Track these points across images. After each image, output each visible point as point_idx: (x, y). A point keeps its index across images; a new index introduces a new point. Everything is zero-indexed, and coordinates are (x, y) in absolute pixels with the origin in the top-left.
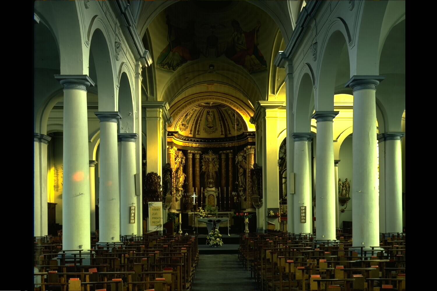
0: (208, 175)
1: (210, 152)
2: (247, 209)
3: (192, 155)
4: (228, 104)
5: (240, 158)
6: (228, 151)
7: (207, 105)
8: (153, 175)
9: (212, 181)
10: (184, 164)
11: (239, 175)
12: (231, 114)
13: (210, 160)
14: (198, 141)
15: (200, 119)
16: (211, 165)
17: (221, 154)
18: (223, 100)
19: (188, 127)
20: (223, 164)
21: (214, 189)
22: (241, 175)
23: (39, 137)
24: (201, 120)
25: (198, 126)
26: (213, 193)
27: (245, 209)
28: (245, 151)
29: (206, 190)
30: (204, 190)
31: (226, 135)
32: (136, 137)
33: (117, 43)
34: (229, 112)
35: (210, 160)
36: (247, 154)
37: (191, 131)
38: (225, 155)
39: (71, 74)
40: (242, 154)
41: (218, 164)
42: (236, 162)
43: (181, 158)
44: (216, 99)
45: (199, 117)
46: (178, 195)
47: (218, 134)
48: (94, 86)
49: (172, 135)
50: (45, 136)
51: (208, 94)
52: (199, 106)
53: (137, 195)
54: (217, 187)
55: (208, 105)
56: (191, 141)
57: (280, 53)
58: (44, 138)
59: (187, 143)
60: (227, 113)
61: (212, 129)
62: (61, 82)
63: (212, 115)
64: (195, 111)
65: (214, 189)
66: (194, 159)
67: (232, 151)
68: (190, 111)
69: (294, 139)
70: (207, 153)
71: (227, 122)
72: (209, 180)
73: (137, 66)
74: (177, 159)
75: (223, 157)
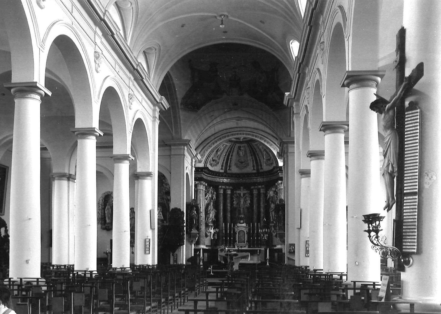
0: (240, 211)
1: (242, 188)
2: (277, 245)
3: (223, 190)
4: (259, 139)
5: (271, 193)
6: (260, 187)
7: (237, 140)
8: (178, 211)
9: (243, 216)
10: (214, 199)
11: (270, 211)
12: (262, 149)
13: (242, 195)
14: (229, 177)
15: (231, 154)
16: (242, 201)
17: (252, 189)
18: (253, 135)
19: (219, 162)
20: (255, 200)
21: (244, 225)
22: (272, 211)
23: (68, 176)
24: (232, 156)
25: (229, 162)
26: (243, 229)
27: (276, 246)
28: (277, 186)
29: (237, 226)
30: (234, 226)
31: (258, 170)
32: (152, 175)
33: (130, 95)
34: (261, 147)
35: (242, 195)
36: (278, 189)
37: (222, 166)
38: (256, 190)
39: (84, 127)
40: (274, 189)
41: (249, 199)
42: (268, 197)
43: (212, 194)
44: (246, 134)
45: (230, 152)
46: (208, 231)
47: (250, 169)
48: (102, 135)
49: (202, 171)
50: (74, 175)
51: (239, 129)
52: (230, 142)
53: (152, 228)
54: (248, 223)
55: (239, 140)
56: (222, 176)
57: (287, 95)
58: (72, 177)
59: (218, 179)
60: (258, 148)
61: (244, 163)
62: (76, 133)
63: (243, 150)
64: (226, 147)
65: (244, 225)
66: (225, 194)
67: (263, 186)
68: (220, 147)
69: (301, 176)
70: (239, 189)
71: (259, 157)
72: (240, 216)
73: (154, 111)
74: (208, 195)
75: (255, 192)
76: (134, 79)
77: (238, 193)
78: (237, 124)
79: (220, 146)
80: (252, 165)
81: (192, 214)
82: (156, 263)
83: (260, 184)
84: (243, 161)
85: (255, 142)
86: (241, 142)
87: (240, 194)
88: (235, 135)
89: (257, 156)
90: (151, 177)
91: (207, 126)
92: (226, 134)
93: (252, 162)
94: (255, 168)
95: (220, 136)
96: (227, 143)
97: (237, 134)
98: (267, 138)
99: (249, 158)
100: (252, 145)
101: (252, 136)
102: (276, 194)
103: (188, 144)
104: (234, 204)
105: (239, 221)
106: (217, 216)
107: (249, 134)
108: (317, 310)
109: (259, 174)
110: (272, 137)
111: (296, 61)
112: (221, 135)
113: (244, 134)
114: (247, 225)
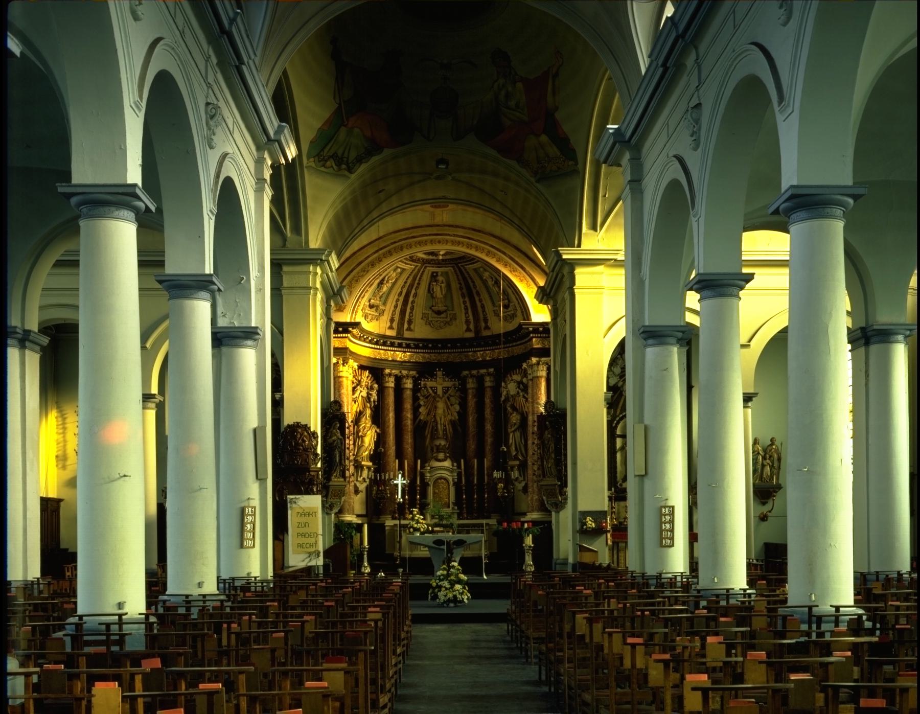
1: (439, 373)
5: (511, 388)
6: (483, 371)
7: (431, 257)
8: (299, 429)
9: (443, 443)
10: (374, 402)
11: (509, 430)
13: (440, 392)
14: (408, 346)
17: (466, 377)
19: (384, 311)
20: (471, 402)
21: (447, 464)
24: (415, 295)
25: (408, 310)
26: (445, 474)
28: (525, 370)
29: (429, 466)
30: (423, 467)
31: (477, 331)
32: (257, 337)
33: (211, 107)
34: (486, 275)
35: (440, 392)
36: (530, 377)
37: (392, 320)
39: (97, 182)
40: (517, 377)
41: (457, 402)
42: (503, 398)
44: (453, 243)
45: (411, 286)
47: (458, 330)
48: (154, 211)
50: (35, 333)
52: (413, 261)
53: (260, 478)
54: (455, 459)
55: (434, 258)
57: (611, 131)
58: (31, 338)
59: (382, 351)
60: (481, 278)
63: (442, 283)
64: (401, 273)
65: (447, 464)
67: (492, 370)
71: (480, 301)
73: (259, 162)
74: (359, 392)
75: (471, 384)
76: (217, 64)
77: (431, 388)
78: (433, 215)
79: (388, 270)
80: (464, 320)
81: (331, 437)
82: (270, 573)
83: (485, 364)
84: (442, 309)
85: (474, 263)
86: (439, 264)
87: (434, 390)
88: (425, 243)
89: (477, 299)
90: (255, 340)
91: (366, 216)
92: (404, 242)
93: (463, 311)
94: (472, 327)
95: (388, 246)
96: (406, 263)
97: (432, 242)
98: (504, 253)
99: (458, 299)
100: (466, 270)
101: (468, 247)
102: (522, 391)
103: (325, 261)
104: (420, 413)
105: (435, 455)
106: (380, 441)
107: (459, 243)
108: (629, 669)
109: (480, 341)
110: (516, 251)
111: (666, 31)
112: (392, 244)
113: (447, 242)
114: (455, 464)
